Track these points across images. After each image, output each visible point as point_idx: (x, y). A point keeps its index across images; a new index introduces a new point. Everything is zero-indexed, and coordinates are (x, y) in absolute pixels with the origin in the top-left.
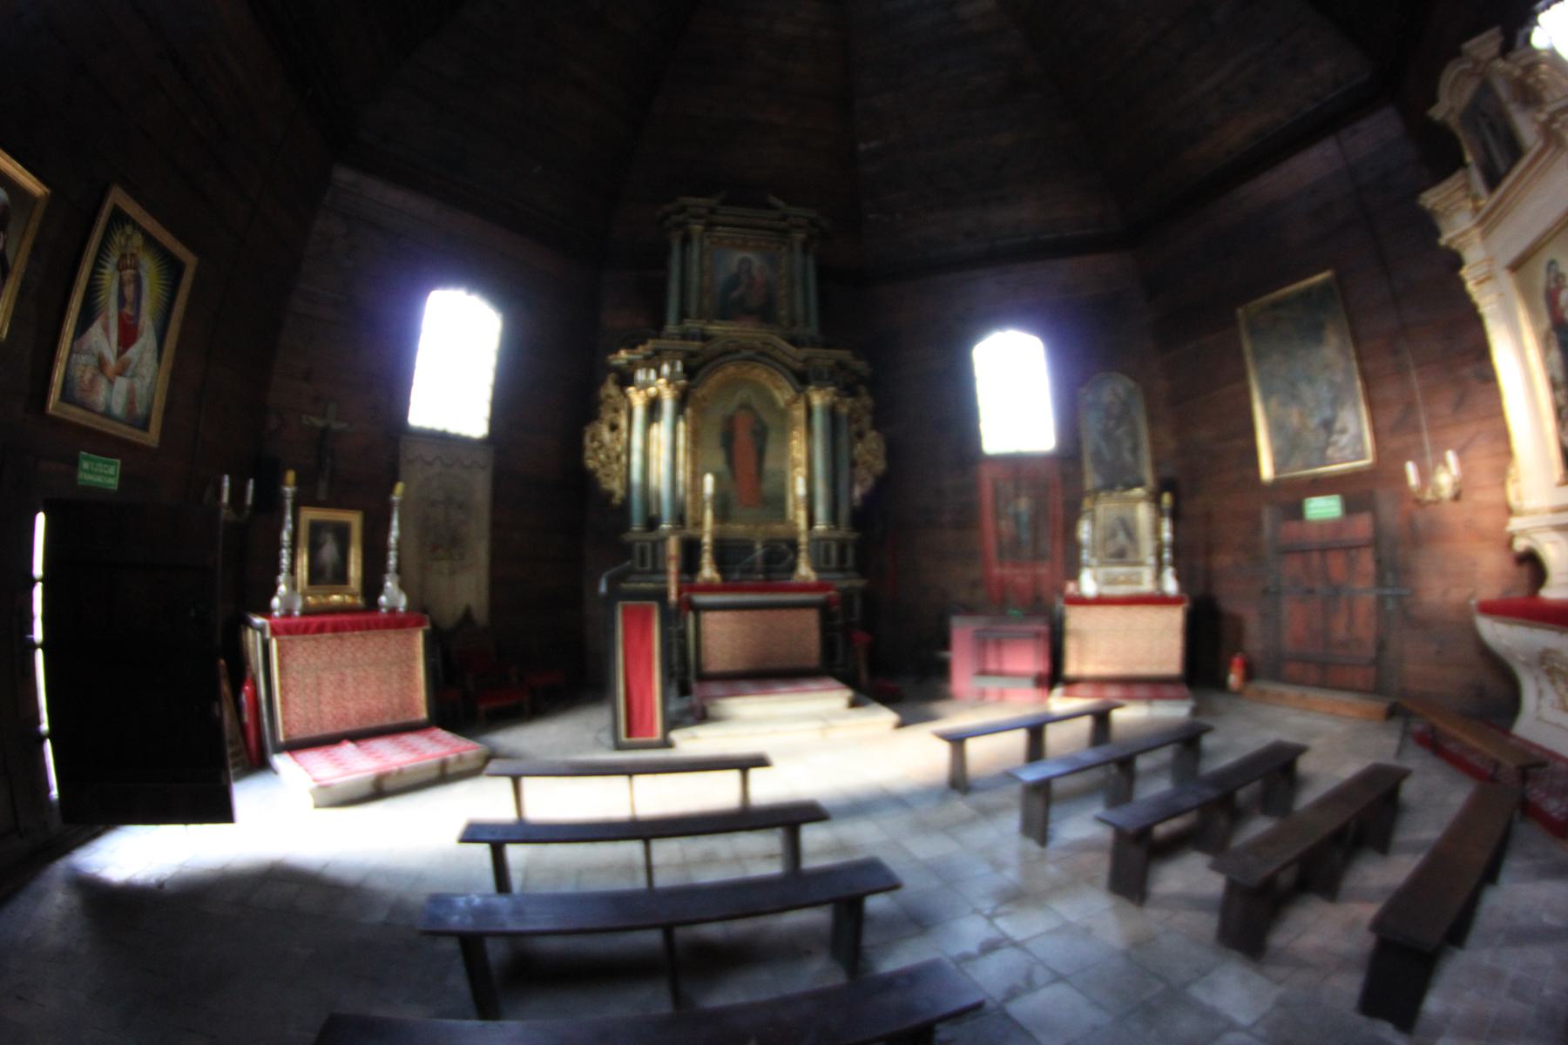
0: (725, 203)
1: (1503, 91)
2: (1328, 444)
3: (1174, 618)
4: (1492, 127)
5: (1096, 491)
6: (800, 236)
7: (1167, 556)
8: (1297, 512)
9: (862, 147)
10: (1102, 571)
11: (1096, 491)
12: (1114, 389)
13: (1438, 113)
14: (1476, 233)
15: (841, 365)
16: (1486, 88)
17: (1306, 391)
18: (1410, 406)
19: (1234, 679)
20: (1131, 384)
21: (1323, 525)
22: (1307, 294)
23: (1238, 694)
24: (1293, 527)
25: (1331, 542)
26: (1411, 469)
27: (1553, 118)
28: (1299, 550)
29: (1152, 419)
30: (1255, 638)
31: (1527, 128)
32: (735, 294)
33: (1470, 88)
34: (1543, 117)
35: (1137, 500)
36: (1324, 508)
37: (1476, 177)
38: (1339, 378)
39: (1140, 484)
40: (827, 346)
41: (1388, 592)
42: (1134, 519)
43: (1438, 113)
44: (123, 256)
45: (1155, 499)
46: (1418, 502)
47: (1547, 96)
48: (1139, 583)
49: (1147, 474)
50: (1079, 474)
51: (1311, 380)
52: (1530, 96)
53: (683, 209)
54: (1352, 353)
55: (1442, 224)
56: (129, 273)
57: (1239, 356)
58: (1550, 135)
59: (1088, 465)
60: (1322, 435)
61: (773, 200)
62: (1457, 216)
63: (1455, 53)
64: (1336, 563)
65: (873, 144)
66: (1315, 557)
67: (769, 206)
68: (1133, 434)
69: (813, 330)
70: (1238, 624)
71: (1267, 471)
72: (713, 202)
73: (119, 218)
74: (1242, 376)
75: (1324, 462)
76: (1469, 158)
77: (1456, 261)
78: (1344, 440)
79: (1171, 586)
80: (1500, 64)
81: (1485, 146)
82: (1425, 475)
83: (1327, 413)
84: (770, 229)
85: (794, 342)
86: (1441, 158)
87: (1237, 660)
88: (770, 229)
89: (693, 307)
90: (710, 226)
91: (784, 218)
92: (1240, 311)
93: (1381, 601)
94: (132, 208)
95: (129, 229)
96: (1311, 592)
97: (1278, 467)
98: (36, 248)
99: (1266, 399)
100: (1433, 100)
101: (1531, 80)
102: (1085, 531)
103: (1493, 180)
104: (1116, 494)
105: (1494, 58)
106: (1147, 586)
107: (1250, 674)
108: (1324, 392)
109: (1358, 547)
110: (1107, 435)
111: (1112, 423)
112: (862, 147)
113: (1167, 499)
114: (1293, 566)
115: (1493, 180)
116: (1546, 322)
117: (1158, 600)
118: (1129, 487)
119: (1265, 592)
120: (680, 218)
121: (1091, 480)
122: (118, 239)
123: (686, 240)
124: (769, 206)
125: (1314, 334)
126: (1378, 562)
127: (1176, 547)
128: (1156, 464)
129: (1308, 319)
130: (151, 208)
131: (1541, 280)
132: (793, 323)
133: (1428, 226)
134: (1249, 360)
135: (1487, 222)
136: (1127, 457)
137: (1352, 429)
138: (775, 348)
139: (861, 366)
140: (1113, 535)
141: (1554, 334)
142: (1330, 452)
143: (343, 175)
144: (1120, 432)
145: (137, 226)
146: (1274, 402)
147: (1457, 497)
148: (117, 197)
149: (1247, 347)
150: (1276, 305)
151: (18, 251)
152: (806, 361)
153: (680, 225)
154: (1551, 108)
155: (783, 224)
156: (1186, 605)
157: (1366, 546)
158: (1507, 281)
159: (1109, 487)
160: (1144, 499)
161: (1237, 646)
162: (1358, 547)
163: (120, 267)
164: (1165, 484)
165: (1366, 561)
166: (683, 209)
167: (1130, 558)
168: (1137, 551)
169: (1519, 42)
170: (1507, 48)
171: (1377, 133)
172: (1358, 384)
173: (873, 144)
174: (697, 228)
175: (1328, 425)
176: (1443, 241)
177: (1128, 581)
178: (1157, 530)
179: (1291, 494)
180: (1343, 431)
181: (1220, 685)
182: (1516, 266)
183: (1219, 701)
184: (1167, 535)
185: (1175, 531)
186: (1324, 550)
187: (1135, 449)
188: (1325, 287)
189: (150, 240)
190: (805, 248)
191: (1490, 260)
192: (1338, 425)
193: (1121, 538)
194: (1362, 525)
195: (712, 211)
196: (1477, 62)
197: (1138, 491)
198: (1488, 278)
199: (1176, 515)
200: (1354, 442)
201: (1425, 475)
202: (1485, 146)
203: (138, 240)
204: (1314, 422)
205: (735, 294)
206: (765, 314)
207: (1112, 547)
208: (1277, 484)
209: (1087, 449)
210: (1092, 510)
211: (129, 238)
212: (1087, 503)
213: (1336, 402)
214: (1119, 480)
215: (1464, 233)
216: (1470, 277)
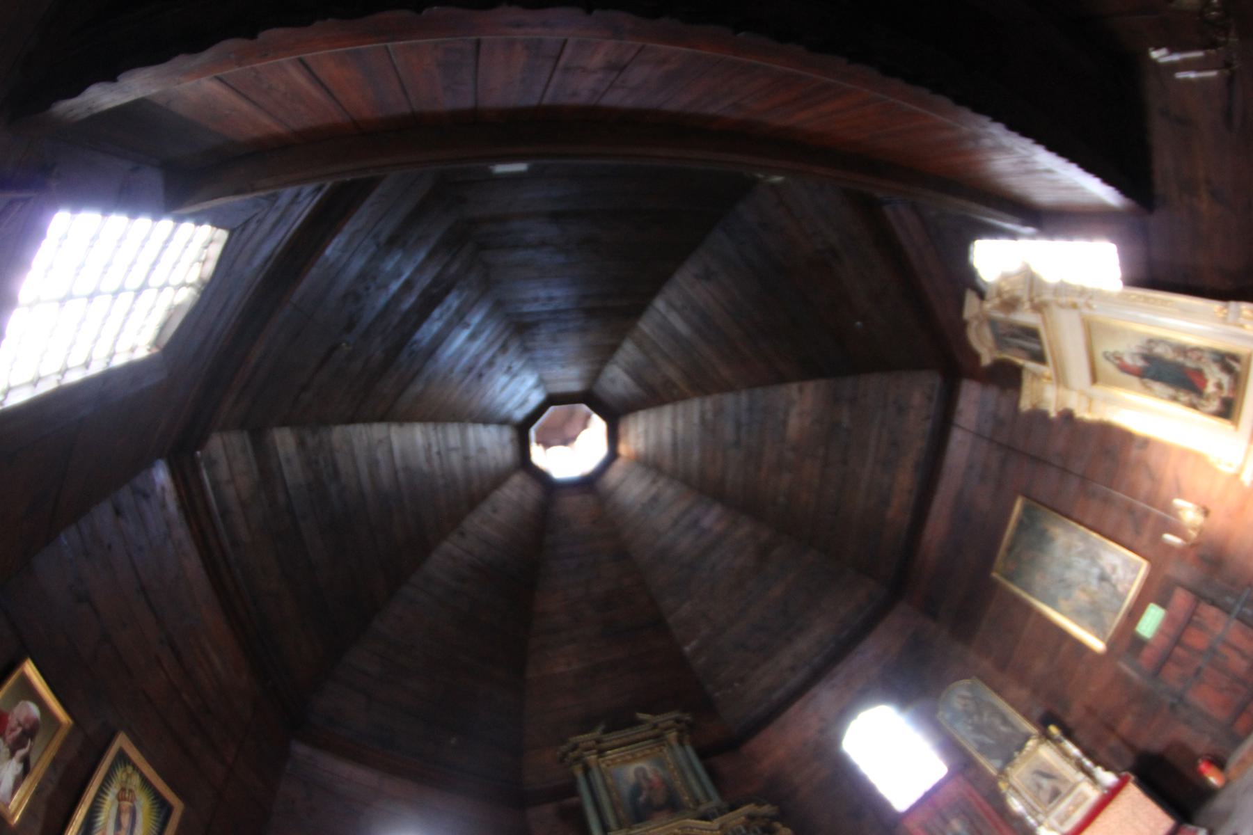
0: (605, 732)
1: (999, 315)
2: (1114, 586)
3: (1133, 794)
4: (1014, 336)
5: (1002, 772)
6: (672, 736)
7: (1088, 763)
8: (1139, 643)
9: (687, 649)
10: (1052, 819)
11: (1002, 772)
12: (959, 695)
13: (986, 360)
14: (1062, 392)
15: (751, 817)
16: (993, 323)
17: (1072, 575)
18: (1130, 510)
19: (1214, 779)
20: (967, 682)
21: (1161, 631)
22: (1021, 525)
23: (1228, 782)
24: (1147, 653)
25: (1176, 632)
26: (1169, 538)
27: (1031, 300)
28: (1166, 658)
29: (999, 691)
30: (1202, 743)
31: (1025, 317)
32: (642, 799)
33: (987, 333)
34: (1027, 305)
35: (1035, 749)
36: (1151, 622)
37: (1031, 365)
38: (1081, 546)
39: (1027, 737)
40: (733, 808)
41: (1238, 608)
42: (1044, 763)
43: (986, 360)
44: (123, 789)
45: (1046, 736)
46: (1194, 545)
47: (1018, 293)
48: (1086, 798)
49: (1028, 727)
50: (980, 770)
51: (1069, 566)
52: (1011, 304)
53: (575, 747)
54: (1074, 524)
55: (1043, 406)
56: (126, 804)
57: (1017, 601)
58: (1038, 308)
59: (982, 760)
60: (1105, 584)
61: (641, 716)
62: (1047, 394)
63: (963, 325)
64: (1195, 639)
65: (694, 643)
66: (1179, 651)
67: (640, 722)
68: (996, 711)
69: (716, 801)
70: (1183, 748)
71: (1097, 645)
72: (597, 733)
73: (122, 758)
74: (1029, 609)
75: (1122, 598)
76: (1020, 362)
77: (1067, 416)
78: (1120, 572)
79: (1109, 778)
80: (988, 306)
81: (1022, 348)
82: (1176, 531)
83: (1096, 571)
84: (650, 738)
85: (705, 817)
86: (1007, 377)
87: (1203, 766)
88: (650, 738)
89: (611, 821)
90: (601, 753)
91: (655, 726)
92: (994, 575)
93: (1241, 618)
94: (134, 754)
95: (130, 769)
96: (1198, 671)
97: (1100, 635)
98: (55, 762)
99: (1053, 604)
100: (976, 357)
101: (1006, 296)
102: (1016, 805)
103: (1040, 358)
104: (1018, 760)
105: (981, 307)
106: (1093, 795)
107: (1219, 763)
108: (1083, 563)
109: (1194, 613)
110: (978, 729)
111: (976, 718)
112: (687, 649)
113: (1053, 730)
114: (1172, 672)
115: (1040, 358)
116: (1135, 380)
117: (1111, 795)
118: (1021, 748)
119: (1173, 707)
120: (576, 753)
121: (991, 766)
122: (120, 775)
123: (587, 770)
124: (640, 722)
125: (1042, 540)
126: (1213, 603)
127: (1087, 753)
128: (1027, 715)
129: (1033, 535)
130: (151, 760)
131: (1107, 368)
132: (698, 803)
133: (1039, 416)
134: (1025, 595)
135: (1061, 379)
136: (1004, 729)
137: (1117, 561)
138: (692, 828)
139: (767, 809)
140: (1039, 787)
141: (1146, 380)
142: (1120, 588)
143: (300, 750)
144: (985, 719)
145: (136, 768)
146: (1063, 604)
147: (1206, 512)
148: (122, 742)
149: (1017, 590)
150: (1010, 550)
151: (39, 759)
152: (721, 827)
153: (578, 759)
154: (1025, 297)
155: (657, 731)
156: (1133, 777)
157: (1196, 607)
158: (1098, 390)
159: (1008, 760)
160: (1040, 743)
161: (1193, 759)
162: (1194, 613)
163: (120, 798)
164: (1043, 722)
165: (1209, 613)
166: (575, 747)
167: (1064, 790)
168: (1065, 781)
169: (983, 286)
170: (981, 295)
171: (973, 402)
172: (1095, 535)
173: (694, 643)
174: (592, 758)
175: (1103, 578)
176: (1053, 414)
177: (1077, 805)
178: (1065, 754)
179: (1126, 640)
180: (1114, 569)
181: (1208, 793)
182: (1094, 378)
183: (1220, 803)
184: (1075, 751)
185: (1077, 744)
186: (1177, 641)
187: (1005, 721)
188: (1026, 510)
189: (146, 782)
190: (681, 743)
191: (1082, 393)
192: (1108, 570)
193: (1046, 783)
194: (1181, 598)
195: (598, 741)
196: (977, 317)
197: (1031, 743)
198: (1090, 400)
199: (1068, 734)
200: (1125, 568)
201: (1176, 531)
202: (1022, 348)
203: (136, 781)
204: (1094, 585)
205: (642, 799)
206: (673, 805)
207: (1045, 796)
208: (1111, 645)
209: (972, 749)
210: (1011, 786)
211: (129, 776)
212: (1002, 786)
213: (1094, 560)
214: (1010, 749)
215: (1058, 398)
216: (1084, 413)
